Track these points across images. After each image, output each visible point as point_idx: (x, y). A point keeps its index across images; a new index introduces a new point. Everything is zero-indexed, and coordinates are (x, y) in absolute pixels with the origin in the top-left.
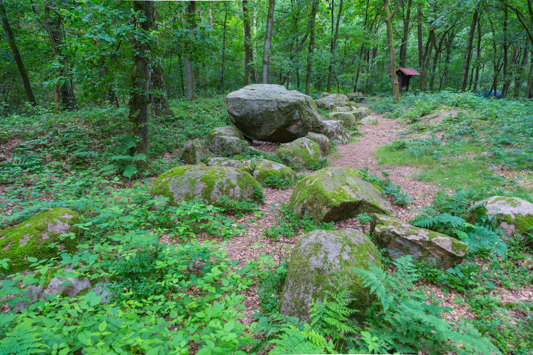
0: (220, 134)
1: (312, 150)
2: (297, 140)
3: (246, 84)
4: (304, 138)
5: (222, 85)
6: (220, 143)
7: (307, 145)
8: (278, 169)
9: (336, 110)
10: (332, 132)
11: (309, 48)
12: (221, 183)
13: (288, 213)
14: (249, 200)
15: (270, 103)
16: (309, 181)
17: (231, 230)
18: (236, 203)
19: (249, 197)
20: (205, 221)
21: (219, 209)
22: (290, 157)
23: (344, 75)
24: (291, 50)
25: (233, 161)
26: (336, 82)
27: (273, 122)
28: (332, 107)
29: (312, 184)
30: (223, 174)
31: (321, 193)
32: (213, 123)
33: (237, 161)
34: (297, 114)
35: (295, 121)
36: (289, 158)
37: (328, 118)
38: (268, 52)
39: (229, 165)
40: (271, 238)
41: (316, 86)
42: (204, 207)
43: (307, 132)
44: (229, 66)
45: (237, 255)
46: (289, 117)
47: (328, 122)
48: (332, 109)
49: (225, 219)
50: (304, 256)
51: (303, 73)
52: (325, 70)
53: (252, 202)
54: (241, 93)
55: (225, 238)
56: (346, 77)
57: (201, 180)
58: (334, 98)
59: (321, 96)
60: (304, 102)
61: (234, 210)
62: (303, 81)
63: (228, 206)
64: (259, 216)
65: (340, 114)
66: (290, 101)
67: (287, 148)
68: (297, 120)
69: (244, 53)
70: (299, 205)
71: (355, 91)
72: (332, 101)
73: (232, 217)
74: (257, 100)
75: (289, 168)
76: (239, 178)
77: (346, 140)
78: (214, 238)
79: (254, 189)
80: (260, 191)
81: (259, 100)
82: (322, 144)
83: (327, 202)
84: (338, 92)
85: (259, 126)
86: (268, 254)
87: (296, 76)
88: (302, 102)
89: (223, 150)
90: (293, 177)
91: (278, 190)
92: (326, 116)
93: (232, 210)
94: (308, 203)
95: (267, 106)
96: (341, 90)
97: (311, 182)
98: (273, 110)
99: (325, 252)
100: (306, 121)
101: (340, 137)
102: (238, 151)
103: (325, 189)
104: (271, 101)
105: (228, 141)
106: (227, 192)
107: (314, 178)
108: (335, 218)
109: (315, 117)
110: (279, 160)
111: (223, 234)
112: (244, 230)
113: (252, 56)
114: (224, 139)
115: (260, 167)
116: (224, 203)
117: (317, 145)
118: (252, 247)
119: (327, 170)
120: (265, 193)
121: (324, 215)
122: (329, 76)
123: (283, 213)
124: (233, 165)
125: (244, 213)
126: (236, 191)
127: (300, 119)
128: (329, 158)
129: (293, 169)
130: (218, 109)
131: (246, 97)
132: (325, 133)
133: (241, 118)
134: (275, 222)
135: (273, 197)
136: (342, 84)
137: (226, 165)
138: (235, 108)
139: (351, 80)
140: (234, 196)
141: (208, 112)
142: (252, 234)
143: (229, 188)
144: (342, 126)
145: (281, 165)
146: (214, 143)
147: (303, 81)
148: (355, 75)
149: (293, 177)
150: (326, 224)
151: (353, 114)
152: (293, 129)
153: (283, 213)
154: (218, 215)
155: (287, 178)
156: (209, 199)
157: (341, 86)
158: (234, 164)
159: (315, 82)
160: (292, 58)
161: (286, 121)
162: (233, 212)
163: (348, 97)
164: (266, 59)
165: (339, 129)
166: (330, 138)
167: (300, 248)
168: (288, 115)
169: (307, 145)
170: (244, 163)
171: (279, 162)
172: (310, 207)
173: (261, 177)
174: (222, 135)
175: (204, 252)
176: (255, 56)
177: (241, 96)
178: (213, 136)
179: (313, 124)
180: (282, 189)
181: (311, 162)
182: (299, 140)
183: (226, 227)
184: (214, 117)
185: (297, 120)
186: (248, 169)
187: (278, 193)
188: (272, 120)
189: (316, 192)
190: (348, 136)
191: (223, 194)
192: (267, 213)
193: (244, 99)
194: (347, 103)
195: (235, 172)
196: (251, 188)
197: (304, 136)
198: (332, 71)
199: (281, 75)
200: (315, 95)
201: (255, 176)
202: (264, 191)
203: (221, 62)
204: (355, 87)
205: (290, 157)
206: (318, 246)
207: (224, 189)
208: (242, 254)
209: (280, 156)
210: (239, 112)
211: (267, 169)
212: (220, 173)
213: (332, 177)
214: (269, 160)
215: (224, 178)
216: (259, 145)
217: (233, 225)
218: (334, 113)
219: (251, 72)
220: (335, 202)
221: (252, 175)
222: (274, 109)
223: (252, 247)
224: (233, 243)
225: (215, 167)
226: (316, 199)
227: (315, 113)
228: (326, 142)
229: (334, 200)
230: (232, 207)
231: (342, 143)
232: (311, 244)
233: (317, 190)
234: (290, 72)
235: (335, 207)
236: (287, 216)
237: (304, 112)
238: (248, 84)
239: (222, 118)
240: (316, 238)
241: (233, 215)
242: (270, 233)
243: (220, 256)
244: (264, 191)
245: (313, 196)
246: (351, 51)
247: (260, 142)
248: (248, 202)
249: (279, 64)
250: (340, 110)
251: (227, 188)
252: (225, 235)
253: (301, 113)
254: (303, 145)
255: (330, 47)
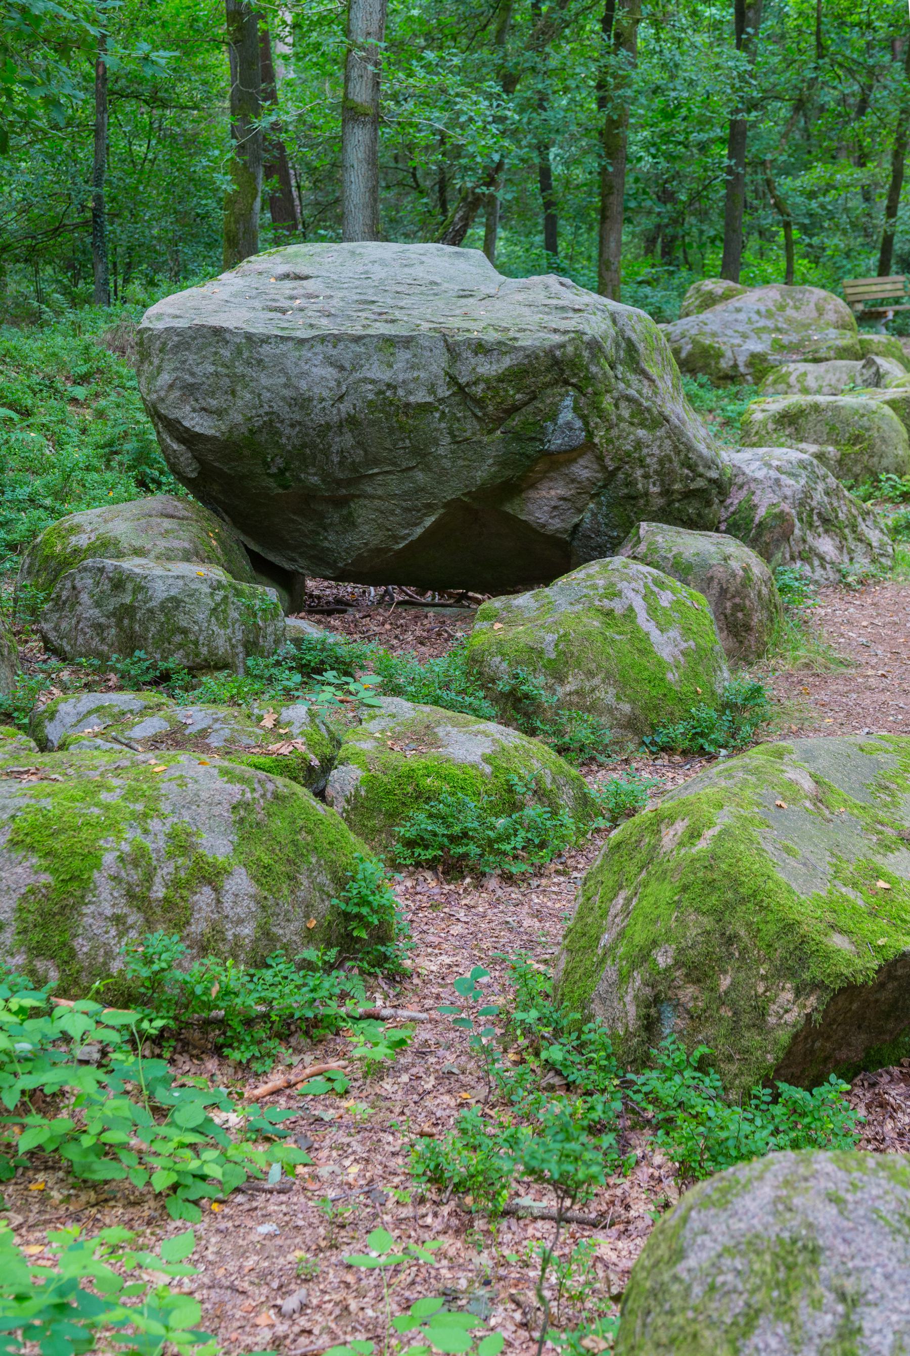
0: (107, 546)
1: (673, 633)
2: (578, 575)
3: (238, 247)
4: (618, 561)
5: (92, 248)
6: (112, 604)
7: (639, 605)
8: (475, 758)
9: (784, 385)
10: (781, 516)
11: (607, 22)
12: (137, 858)
13: (558, 1032)
14: (311, 954)
15: (403, 356)
16: (680, 826)
17: (210, 1155)
18: (234, 974)
19: (309, 936)
20: (43, 1101)
21: (129, 1017)
22: (541, 680)
23: (819, 172)
24: (500, 33)
25: (195, 714)
26: (769, 218)
27: (428, 468)
28: (759, 369)
29: (702, 846)
30: (147, 802)
31: (757, 899)
32: (54, 477)
33: (223, 711)
34: (567, 416)
35: (556, 462)
36: (536, 683)
37: (748, 436)
38: (371, 51)
39: (175, 738)
40: (464, 1196)
41: (651, 242)
42: (34, 1013)
43: (629, 526)
44: (131, 137)
45: (256, 1310)
46: (518, 438)
47: (735, 458)
48: (759, 378)
49: (167, 1081)
50: (712, 1324)
51: (573, 166)
52: (703, 147)
53: (330, 967)
54: (225, 299)
55: (174, 1205)
56: (830, 187)
57: (14, 844)
58: (769, 315)
59: (691, 300)
60: (608, 346)
61: (221, 1023)
62: (581, 214)
63: (187, 999)
64: (381, 1053)
65: (816, 408)
66: (525, 341)
67: (519, 622)
68: (572, 454)
69: (222, 62)
70: (624, 978)
71: (883, 269)
72: (758, 331)
73: (212, 1064)
74: (323, 339)
75: (535, 745)
76: (246, 823)
77: (862, 565)
78: (101, 1203)
79: (341, 883)
80: (376, 900)
81: (337, 339)
82: (723, 591)
83: (796, 956)
84: (789, 276)
85: (341, 495)
86: (450, 1297)
87: (533, 186)
88: (595, 346)
89: (130, 643)
90: (566, 799)
91: (479, 885)
92: (727, 423)
93: (208, 1022)
94: (678, 964)
95: (386, 376)
96: (802, 265)
97: (694, 834)
98: (421, 397)
99: (842, 1297)
100: (624, 459)
101: (826, 545)
102: (222, 647)
103: (781, 876)
104: (407, 342)
105: (160, 592)
106: (174, 914)
107: (706, 806)
108: (843, 1054)
109: (676, 435)
110: (478, 699)
111: (161, 1182)
112: (288, 1150)
113: (269, 75)
114: (131, 577)
115: (367, 746)
116: (156, 982)
117: (701, 603)
118: (346, 1255)
119: (780, 754)
120: (401, 902)
121: (784, 1036)
122: (734, 185)
123: (527, 1031)
124: (199, 742)
125: (284, 1037)
126: (227, 901)
127: (589, 446)
128: (770, 677)
129: (562, 750)
130: (80, 392)
131: (259, 323)
132: (741, 527)
133: (230, 448)
134: (482, 1091)
135: (457, 929)
136: (804, 229)
137: (154, 743)
138: (190, 390)
139: (857, 203)
140: (217, 932)
141: (26, 413)
142: (342, 1168)
143: (187, 885)
144: (832, 481)
145: (493, 727)
146: (74, 600)
147: (581, 214)
148: (879, 170)
149: (566, 799)
150: (799, 1094)
151: (892, 404)
152: (545, 507)
153: (527, 1031)
154: (121, 1058)
155: (533, 811)
156: (64, 955)
157: (804, 241)
158: (204, 733)
159: (646, 223)
160: (509, 82)
161: (503, 463)
162: (214, 1034)
163: (851, 304)
164: (361, 94)
165: (819, 496)
166: (766, 555)
167: (680, 1269)
168: (515, 421)
169: (639, 605)
170: (268, 723)
171: (476, 712)
172: (691, 990)
173: (377, 810)
174: (120, 555)
175: (62, 1308)
176: (285, 73)
177: (230, 320)
178: (66, 563)
179: (664, 475)
180: (508, 878)
181: (669, 706)
182: (588, 576)
183: (178, 1138)
184: (59, 444)
185: (572, 454)
186: (294, 762)
187: (480, 900)
188: (421, 453)
189: (725, 897)
190: (874, 536)
191: (150, 925)
192: (424, 1034)
193: (249, 337)
194: (848, 339)
195: (220, 783)
196: (324, 878)
197: (604, 549)
198: (749, 156)
199: (443, 185)
200: (656, 295)
201: (341, 804)
202: (398, 894)
203: (86, 113)
204: (888, 241)
205: (541, 680)
206: (796, 1257)
207: (159, 892)
208: (290, 1304)
209: (479, 675)
210: (219, 413)
211: (411, 760)
212: (132, 794)
213: (818, 800)
214: (413, 698)
215: (154, 825)
216: (338, 607)
217: (218, 1117)
218: (777, 404)
219: (269, 172)
220: (851, 955)
221: (321, 795)
222: (432, 390)
223: (346, 1255)
224: (224, 1233)
225: (100, 758)
226: (730, 940)
227: (676, 408)
228: (747, 581)
229: (838, 941)
230: (208, 1006)
231: (842, 583)
232: (751, 1245)
233: (736, 883)
234: (499, 166)
235: (850, 990)
236: (555, 1053)
237: (607, 402)
238: (254, 251)
239: (110, 450)
240: (782, 1206)
241: (218, 1051)
242: (460, 1162)
243: (156, 1328)
244: (398, 894)
245: (708, 922)
246: (853, 35)
247: (347, 589)
248: (307, 966)
249: (439, 118)
250: (811, 382)
251: (175, 884)
252: (174, 1188)
253: (588, 411)
254: (617, 606)
255: (729, 14)
